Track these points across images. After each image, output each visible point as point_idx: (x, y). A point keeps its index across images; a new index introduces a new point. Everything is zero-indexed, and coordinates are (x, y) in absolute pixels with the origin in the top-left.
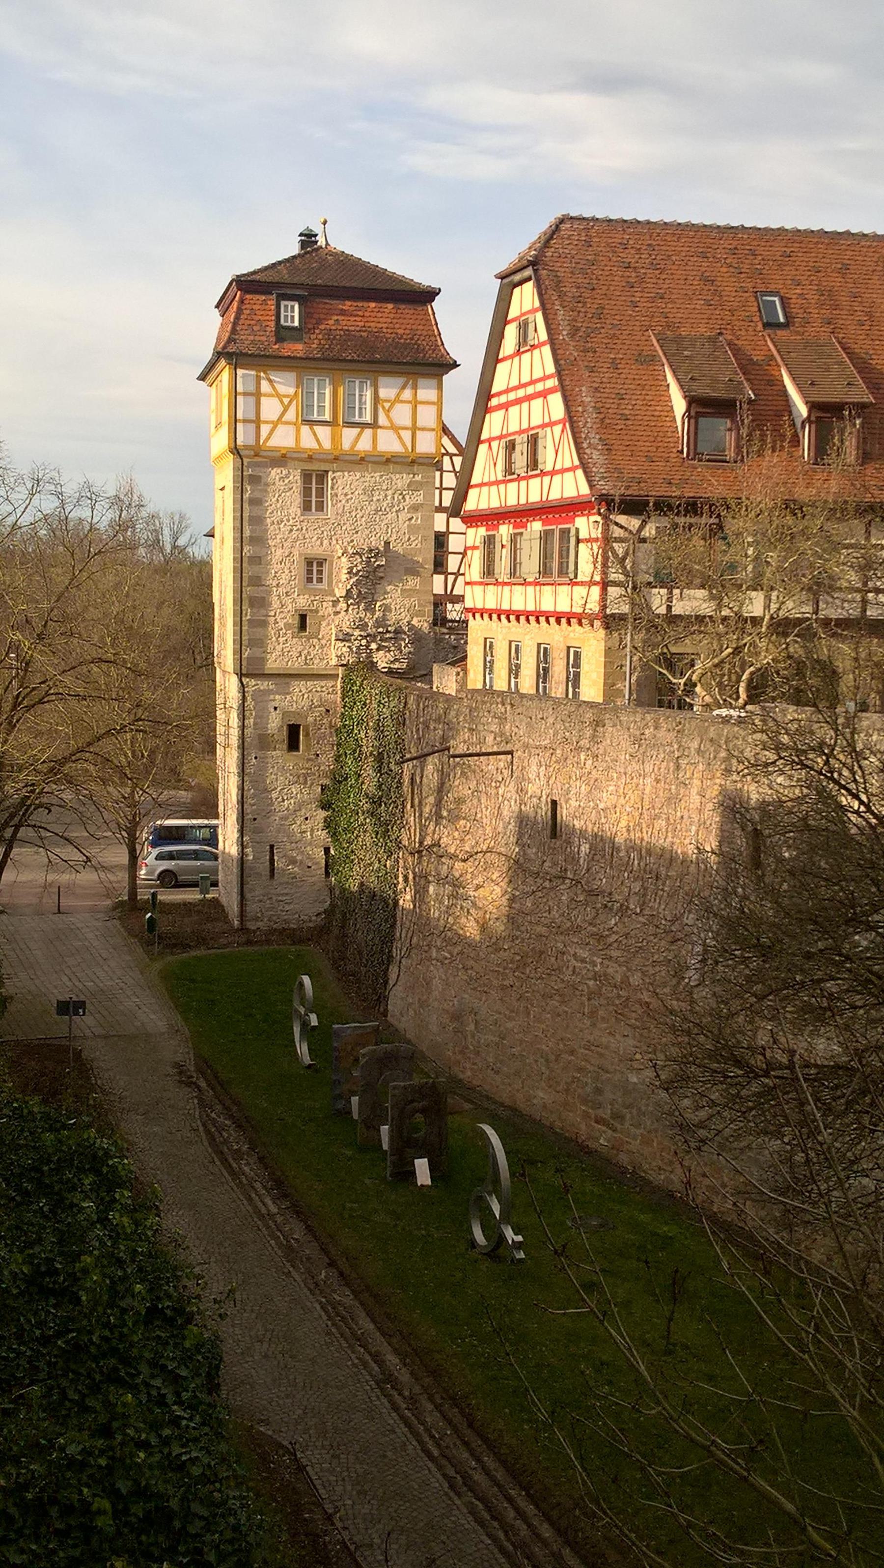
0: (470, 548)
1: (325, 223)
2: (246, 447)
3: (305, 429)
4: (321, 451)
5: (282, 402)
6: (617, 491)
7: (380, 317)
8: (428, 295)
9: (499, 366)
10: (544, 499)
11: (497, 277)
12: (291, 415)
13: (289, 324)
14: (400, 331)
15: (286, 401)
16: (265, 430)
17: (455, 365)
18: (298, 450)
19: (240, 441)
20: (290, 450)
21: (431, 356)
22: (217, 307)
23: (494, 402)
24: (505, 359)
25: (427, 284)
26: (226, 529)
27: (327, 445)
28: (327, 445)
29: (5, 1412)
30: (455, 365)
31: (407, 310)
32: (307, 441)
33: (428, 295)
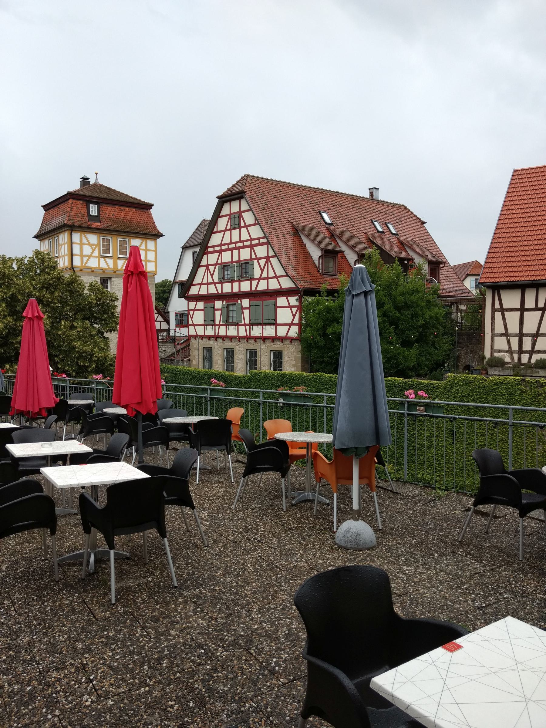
0: (191, 310)
1: (96, 174)
2: (77, 267)
3: (102, 260)
4: (109, 269)
5: (92, 248)
6: (303, 285)
7: (131, 214)
8: (149, 206)
9: (213, 235)
10: (253, 289)
11: (217, 198)
12: (96, 253)
13: (93, 214)
14: (139, 220)
15: (94, 247)
16: (85, 259)
17: (162, 235)
18: (99, 268)
19: (74, 264)
20: (96, 269)
21: (152, 231)
22: (47, 207)
23: (210, 250)
24: (218, 232)
25: (147, 202)
26: (120, 298)
27: (111, 266)
28: (111, 266)
29: (543, 540)
30: (162, 235)
31: (141, 212)
32: (103, 265)
33: (149, 206)
